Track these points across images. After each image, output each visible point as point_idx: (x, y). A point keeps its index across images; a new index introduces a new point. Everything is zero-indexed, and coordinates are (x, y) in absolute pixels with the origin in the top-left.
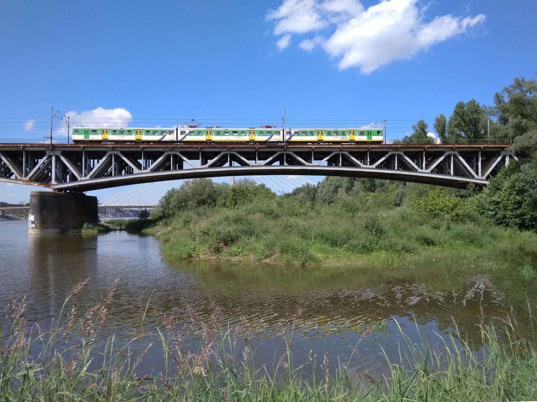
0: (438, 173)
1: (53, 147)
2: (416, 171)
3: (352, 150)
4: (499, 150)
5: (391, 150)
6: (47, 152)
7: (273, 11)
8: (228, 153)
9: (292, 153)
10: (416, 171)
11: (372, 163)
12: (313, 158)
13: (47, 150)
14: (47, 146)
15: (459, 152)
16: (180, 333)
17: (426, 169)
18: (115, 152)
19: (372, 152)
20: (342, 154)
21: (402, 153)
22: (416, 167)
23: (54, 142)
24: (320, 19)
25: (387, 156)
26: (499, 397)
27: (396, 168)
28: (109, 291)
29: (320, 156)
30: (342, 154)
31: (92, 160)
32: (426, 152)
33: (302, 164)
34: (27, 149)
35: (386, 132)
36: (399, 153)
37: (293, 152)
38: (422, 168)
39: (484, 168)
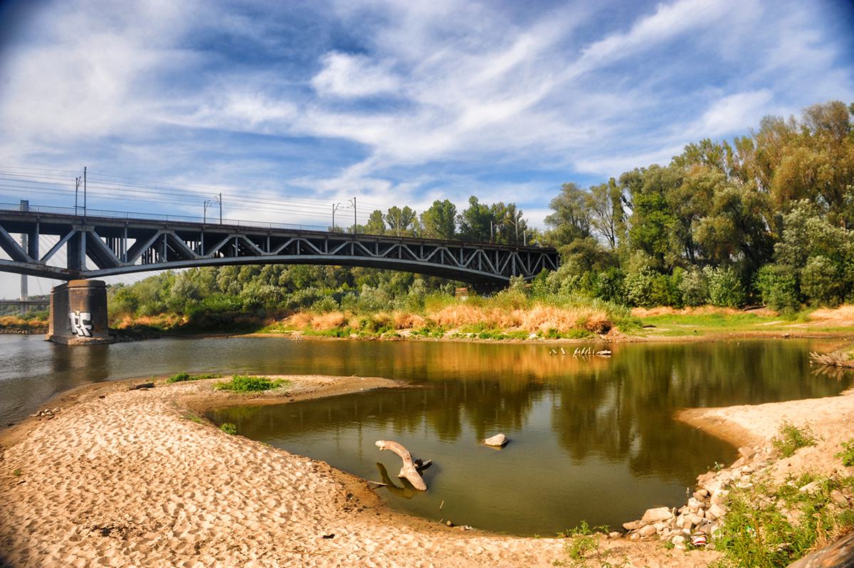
0: (388, 257)
1: (84, 220)
2: (260, 254)
3: (409, 243)
4: (69, 222)
5: (233, 232)
6: (74, 227)
7: (343, 169)
8: (235, 238)
9: (359, 243)
10: (260, 254)
11: (329, 250)
12: (38, 230)
13: (75, 224)
14: (76, 218)
15: (485, 250)
16: (757, 213)
17: (328, 251)
18: (168, 232)
19: (502, 251)
20: (300, 241)
21: (446, 249)
22: (259, 250)
23: (89, 214)
24: (390, 188)
25: (394, 246)
26: (653, 362)
27: (400, 257)
28: (261, 470)
29: (383, 247)
30: (300, 241)
31: (116, 239)
32: (379, 244)
33: (370, 256)
34: (43, 221)
35: (78, 197)
36: (445, 248)
37: (361, 242)
38: (266, 251)
39: (362, 252)
